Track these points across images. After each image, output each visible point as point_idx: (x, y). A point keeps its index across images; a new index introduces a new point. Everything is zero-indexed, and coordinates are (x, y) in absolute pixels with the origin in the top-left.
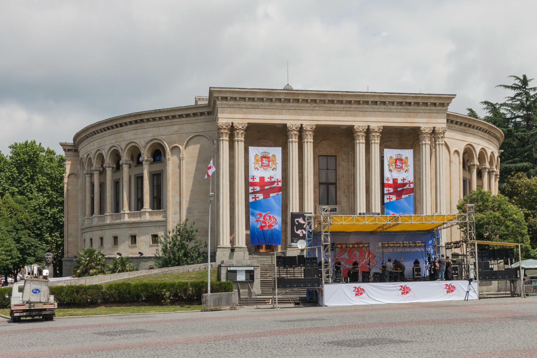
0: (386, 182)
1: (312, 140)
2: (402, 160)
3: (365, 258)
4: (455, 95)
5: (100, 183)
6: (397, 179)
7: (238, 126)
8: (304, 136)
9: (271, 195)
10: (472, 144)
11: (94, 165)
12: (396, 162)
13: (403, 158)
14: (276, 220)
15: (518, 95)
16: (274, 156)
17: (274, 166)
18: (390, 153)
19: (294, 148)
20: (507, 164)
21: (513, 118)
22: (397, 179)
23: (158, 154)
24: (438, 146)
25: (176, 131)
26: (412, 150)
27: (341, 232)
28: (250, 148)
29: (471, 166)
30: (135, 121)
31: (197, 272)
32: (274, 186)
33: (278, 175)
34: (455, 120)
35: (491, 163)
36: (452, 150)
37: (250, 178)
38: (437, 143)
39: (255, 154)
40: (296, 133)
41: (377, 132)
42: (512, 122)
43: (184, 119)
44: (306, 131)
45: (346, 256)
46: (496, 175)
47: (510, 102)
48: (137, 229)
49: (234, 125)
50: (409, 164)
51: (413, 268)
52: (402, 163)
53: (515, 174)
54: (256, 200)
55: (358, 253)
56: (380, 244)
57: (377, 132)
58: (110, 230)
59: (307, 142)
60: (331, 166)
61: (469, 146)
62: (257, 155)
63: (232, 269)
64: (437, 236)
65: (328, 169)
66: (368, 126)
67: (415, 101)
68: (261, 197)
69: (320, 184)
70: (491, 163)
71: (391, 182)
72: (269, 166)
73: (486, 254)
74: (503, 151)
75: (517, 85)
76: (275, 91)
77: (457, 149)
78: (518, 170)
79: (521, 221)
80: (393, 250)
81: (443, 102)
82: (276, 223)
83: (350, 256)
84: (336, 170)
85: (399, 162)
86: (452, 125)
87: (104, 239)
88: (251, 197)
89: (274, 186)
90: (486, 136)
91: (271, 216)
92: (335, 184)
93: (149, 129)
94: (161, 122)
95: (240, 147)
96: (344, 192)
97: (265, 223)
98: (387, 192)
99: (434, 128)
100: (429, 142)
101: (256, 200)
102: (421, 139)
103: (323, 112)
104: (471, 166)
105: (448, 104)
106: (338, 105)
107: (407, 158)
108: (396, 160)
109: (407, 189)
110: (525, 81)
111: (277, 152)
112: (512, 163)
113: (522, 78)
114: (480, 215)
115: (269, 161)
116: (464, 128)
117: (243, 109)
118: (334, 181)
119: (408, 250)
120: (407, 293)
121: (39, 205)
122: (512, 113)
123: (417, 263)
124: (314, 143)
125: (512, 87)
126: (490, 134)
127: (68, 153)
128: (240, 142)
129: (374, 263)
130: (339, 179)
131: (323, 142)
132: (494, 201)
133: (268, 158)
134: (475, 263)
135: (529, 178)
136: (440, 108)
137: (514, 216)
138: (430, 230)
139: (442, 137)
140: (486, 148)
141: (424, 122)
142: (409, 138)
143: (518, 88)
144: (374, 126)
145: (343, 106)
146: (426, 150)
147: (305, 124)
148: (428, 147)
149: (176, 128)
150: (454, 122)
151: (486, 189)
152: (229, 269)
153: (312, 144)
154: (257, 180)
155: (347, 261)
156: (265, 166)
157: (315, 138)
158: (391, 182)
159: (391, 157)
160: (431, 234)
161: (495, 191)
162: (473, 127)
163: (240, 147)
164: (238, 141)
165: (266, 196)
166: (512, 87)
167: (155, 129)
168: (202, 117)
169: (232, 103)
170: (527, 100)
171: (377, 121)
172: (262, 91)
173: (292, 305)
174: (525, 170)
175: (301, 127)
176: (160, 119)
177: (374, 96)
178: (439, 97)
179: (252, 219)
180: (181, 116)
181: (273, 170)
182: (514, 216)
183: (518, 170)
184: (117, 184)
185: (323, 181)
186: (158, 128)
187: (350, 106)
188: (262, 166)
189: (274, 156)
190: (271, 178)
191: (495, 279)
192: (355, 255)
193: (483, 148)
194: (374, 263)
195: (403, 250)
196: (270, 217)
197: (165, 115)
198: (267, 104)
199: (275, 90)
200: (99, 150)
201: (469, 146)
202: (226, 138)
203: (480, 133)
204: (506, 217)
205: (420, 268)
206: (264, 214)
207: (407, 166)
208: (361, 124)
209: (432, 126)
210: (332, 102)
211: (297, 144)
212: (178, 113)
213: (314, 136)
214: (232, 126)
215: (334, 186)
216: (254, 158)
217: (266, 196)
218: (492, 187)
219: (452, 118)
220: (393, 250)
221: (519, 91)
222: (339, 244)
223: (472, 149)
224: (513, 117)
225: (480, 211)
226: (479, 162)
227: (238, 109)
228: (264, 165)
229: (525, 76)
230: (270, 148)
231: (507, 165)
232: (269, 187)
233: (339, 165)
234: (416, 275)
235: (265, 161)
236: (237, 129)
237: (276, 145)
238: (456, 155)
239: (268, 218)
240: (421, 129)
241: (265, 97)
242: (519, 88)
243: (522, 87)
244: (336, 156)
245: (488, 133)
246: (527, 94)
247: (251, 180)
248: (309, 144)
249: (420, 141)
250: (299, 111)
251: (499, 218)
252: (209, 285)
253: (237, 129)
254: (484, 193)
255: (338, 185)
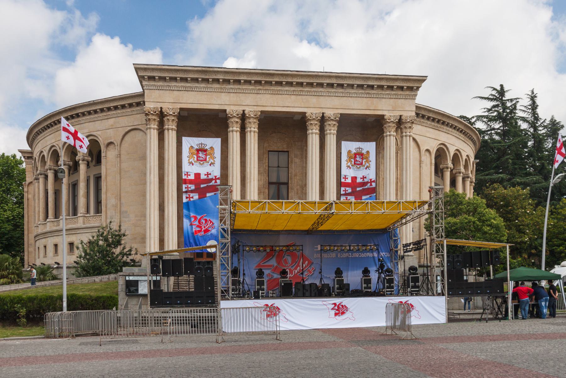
0: (343, 180)
1: (256, 130)
2: (362, 155)
3: (298, 266)
4: (427, 77)
5: (55, 190)
6: (356, 178)
7: (168, 111)
8: (248, 125)
9: (208, 195)
10: (446, 144)
11: (39, 168)
12: (355, 157)
13: (364, 152)
14: (213, 224)
15: (494, 106)
16: (212, 148)
17: (212, 161)
18: (349, 146)
19: (235, 138)
20: (482, 176)
21: (488, 131)
22: (356, 178)
23: (96, 154)
24: (404, 138)
25: (112, 125)
26: (374, 143)
27: (267, 231)
28: (184, 139)
29: (443, 169)
30: (70, 116)
31: (105, 282)
32: (211, 184)
33: (216, 171)
34: (427, 114)
35: (466, 167)
36: (423, 148)
37: (183, 175)
38: (404, 134)
39: (189, 146)
40: (237, 120)
41: (332, 120)
42: (487, 134)
43: (119, 111)
44: (249, 118)
45: (273, 262)
46: (471, 182)
47: (486, 114)
48: (74, 235)
49: (163, 110)
50: (370, 159)
51: (362, 279)
52: (362, 159)
53: (490, 185)
54: (190, 200)
55: (289, 259)
56: (319, 248)
57: (332, 120)
58: (51, 238)
59: (250, 132)
60: (283, 163)
61: (442, 146)
62: (192, 147)
63: (131, 278)
64: (395, 236)
65: (278, 167)
66: (323, 113)
67: (379, 84)
68: (196, 197)
69: (270, 183)
70: (466, 167)
71: (349, 180)
72: (206, 160)
73: (459, 259)
74: (478, 161)
75: (494, 95)
76: (211, 69)
77: (429, 148)
78: (493, 182)
79: (500, 226)
80: (337, 255)
81: (411, 85)
82: (213, 228)
83: (279, 262)
84: (288, 167)
85: (358, 159)
86: (422, 120)
87: (47, 247)
88: (184, 196)
89: (211, 184)
90: (462, 136)
91: (208, 219)
92: (287, 184)
93: (85, 125)
94: (96, 116)
95: (171, 137)
96: (297, 193)
97: (201, 227)
98: (344, 192)
99: (401, 116)
100: (395, 134)
101: (190, 200)
102: (385, 130)
103: (269, 95)
104: (443, 169)
105: (418, 88)
106: (287, 88)
107: (368, 152)
108: (356, 154)
109: (368, 189)
110: (502, 92)
111: (214, 143)
112: (487, 175)
113: (499, 88)
114: (452, 220)
115: (206, 155)
116: (436, 125)
117: (175, 92)
118: (286, 181)
119: (357, 255)
120: (343, 313)
121: (13, 216)
122: (488, 125)
123: (366, 272)
124: (259, 133)
125: (487, 99)
126: (466, 135)
127: (27, 160)
128: (170, 131)
129: (310, 272)
130: (291, 179)
131: (274, 135)
132: (469, 203)
133: (205, 151)
134: (442, 272)
135: (505, 189)
136: (408, 93)
137: (493, 221)
138: (385, 229)
139: (410, 127)
140: (461, 150)
141: (386, 107)
142: (369, 128)
143: (495, 99)
144: (329, 113)
145: (292, 89)
146: (391, 141)
147: (247, 110)
148: (393, 139)
149: (111, 121)
150: (427, 115)
151: (460, 190)
152: (127, 278)
153: (257, 135)
154: (192, 177)
155: (275, 270)
156: (202, 161)
157: (260, 127)
158: (349, 180)
159: (349, 152)
160: (385, 235)
161: (470, 194)
162: (447, 125)
163: (171, 137)
164: (168, 130)
165: (202, 195)
166: (487, 99)
167: (91, 123)
168: (138, 108)
169: (161, 83)
170: (504, 112)
171: (334, 105)
172: (196, 69)
173: (188, 327)
174: (501, 181)
175: (244, 114)
176: (95, 112)
177: (330, 77)
178: (407, 79)
179: (186, 223)
180: (116, 108)
181: (210, 165)
182: (493, 221)
183: (493, 182)
184: (74, 186)
185: (274, 180)
186: (93, 123)
187: (301, 89)
188: (197, 160)
189: (212, 148)
190: (208, 174)
191: (478, 294)
192: (286, 262)
193: (457, 150)
194: (310, 272)
195: (350, 255)
196: (206, 220)
197: (100, 107)
198: (203, 85)
199: (211, 67)
200: (54, 146)
201: (442, 146)
202: (154, 125)
203: (455, 132)
204: (484, 221)
205: (370, 279)
206: (199, 217)
207: (368, 161)
208: (315, 111)
209: (398, 114)
210: (279, 83)
211: (238, 134)
212: (112, 105)
213: (259, 124)
214: (161, 112)
215: (286, 186)
216: (188, 150)
217: (202, 195)
218: (467, 190)
219: (423, 112)
220: (337, 255)
221: (495, 103)
222: (262, 246)
223: (445, 149)
224: (489, 129)
225: (454, 215)
226: (454, 165)
227: (168, 92)
228: (198, 157)
229: (502, 86)
230: (207, 139)
231: (483, 178)
232: (205, 185)
233: (292, 162)
234: (365, 288)
235: (201, 154)
236: (166, 116)
237: (215, 135)
238: (427, 154)
239: (204, 222)
240: (385, 117)
241: (200, 76)
242: (495, 99)
243: (498, 98)
244: (288, 152)
245: (463, 134)
246: (504, 104)
247: (184, 177)
248: (252, 133)
249: (383, 133)
250: (241, 95)
251: (474, 222)
252: (65, 300)
253: (166, 116)
254: (458, 195)
255: (290, 185)
